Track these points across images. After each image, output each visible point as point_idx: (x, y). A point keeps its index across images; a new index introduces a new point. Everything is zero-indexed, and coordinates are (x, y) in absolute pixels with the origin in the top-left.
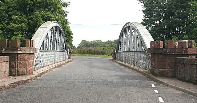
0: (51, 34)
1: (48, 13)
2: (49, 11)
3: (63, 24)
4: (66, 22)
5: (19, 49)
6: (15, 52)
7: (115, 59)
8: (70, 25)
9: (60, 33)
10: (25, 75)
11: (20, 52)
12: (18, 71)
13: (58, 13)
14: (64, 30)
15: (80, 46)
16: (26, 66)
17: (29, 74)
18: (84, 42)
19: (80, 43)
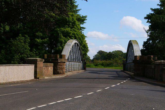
0: (73, 50)
1: (68, 29)
2: (68, 27)
3: (80, 39)
4: (83, 37)
5: (59, 60)
6: (57, 61)
7: (125, 70)
8: (86, 39)
9: (78, 47)
10: (61, 74)
11: (59, 61)
12: (58, 72)
13: (78, 37)
14: (81, 45)
15: (96, 58)
16: (62, 69)
17: (63, 73)
18: (101, 53)
19: (96, 53)
